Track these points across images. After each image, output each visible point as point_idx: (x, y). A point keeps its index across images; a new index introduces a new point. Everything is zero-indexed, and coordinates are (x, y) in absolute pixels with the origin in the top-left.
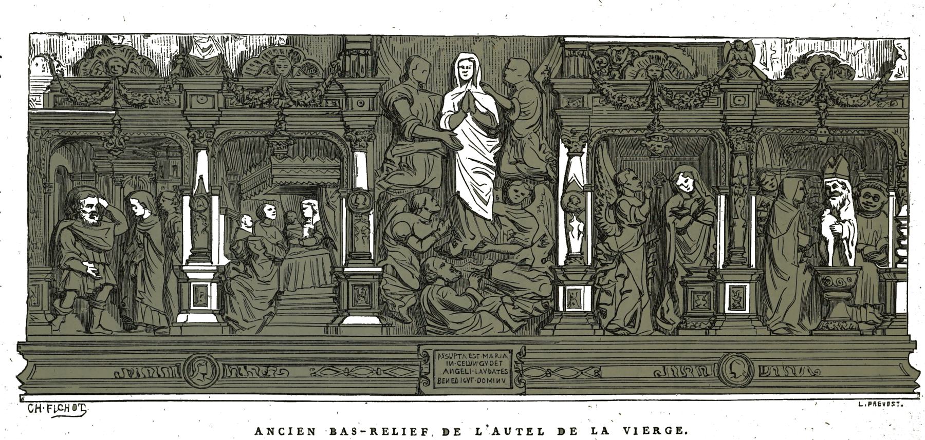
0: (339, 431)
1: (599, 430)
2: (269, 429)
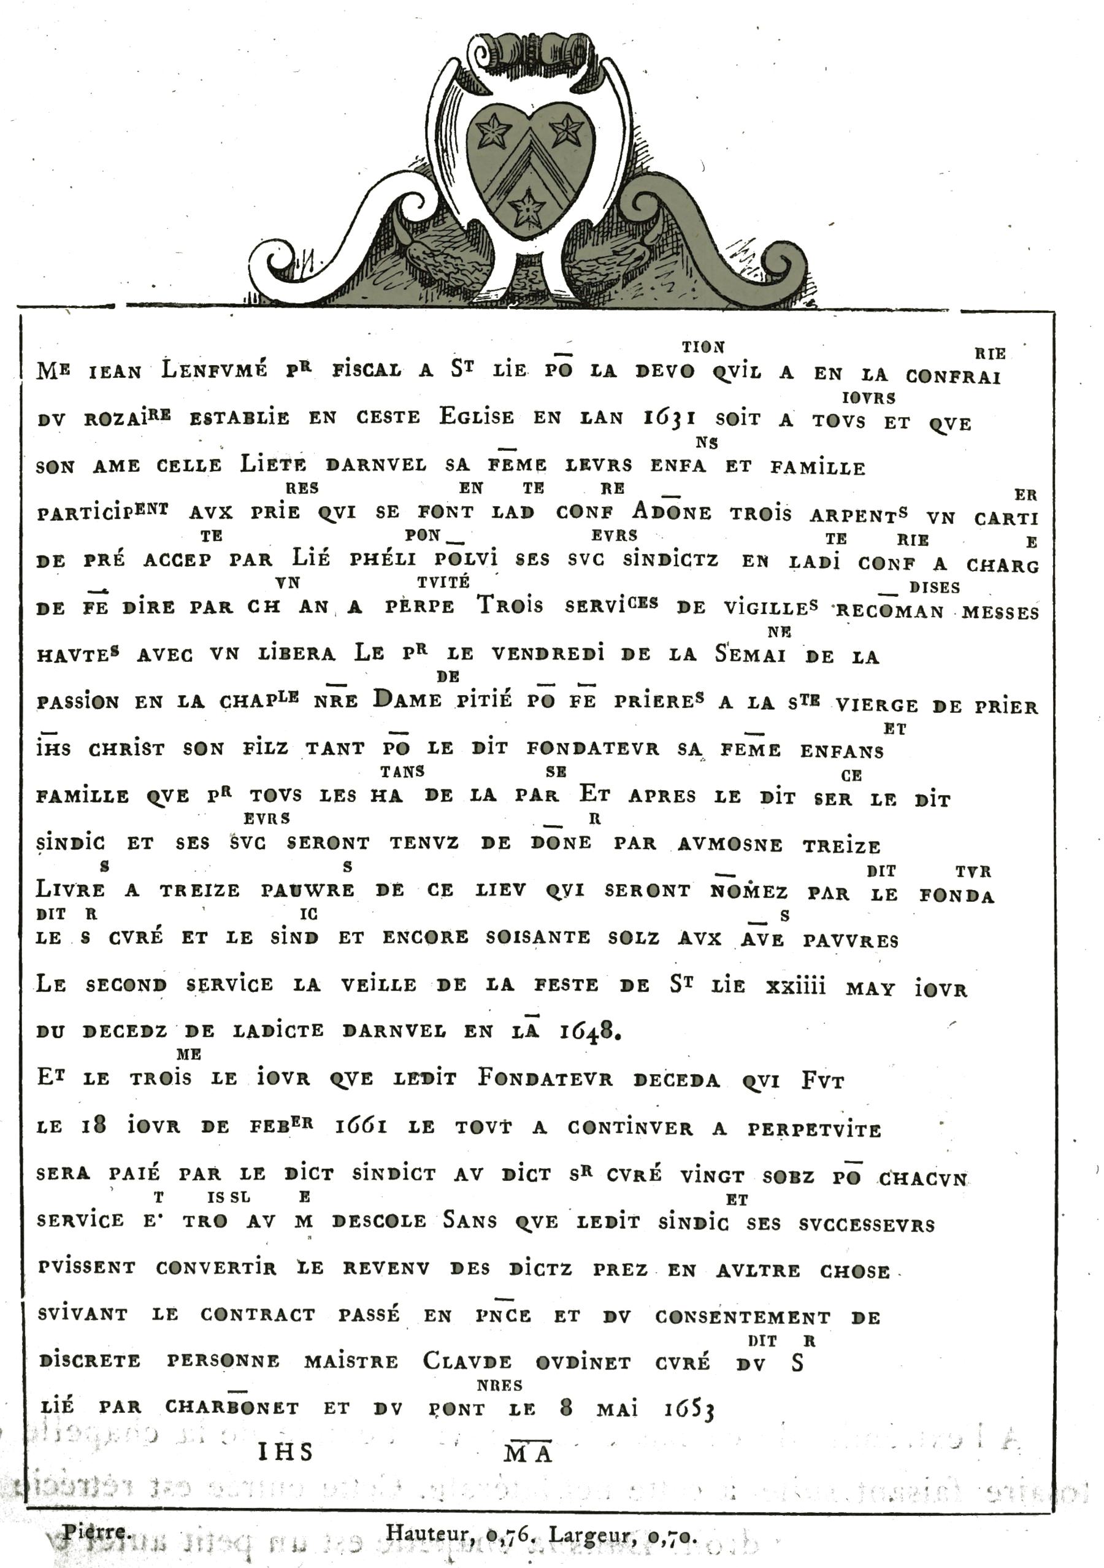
0: (274, 1314)
1: (499, 982)
2: (318, 698)
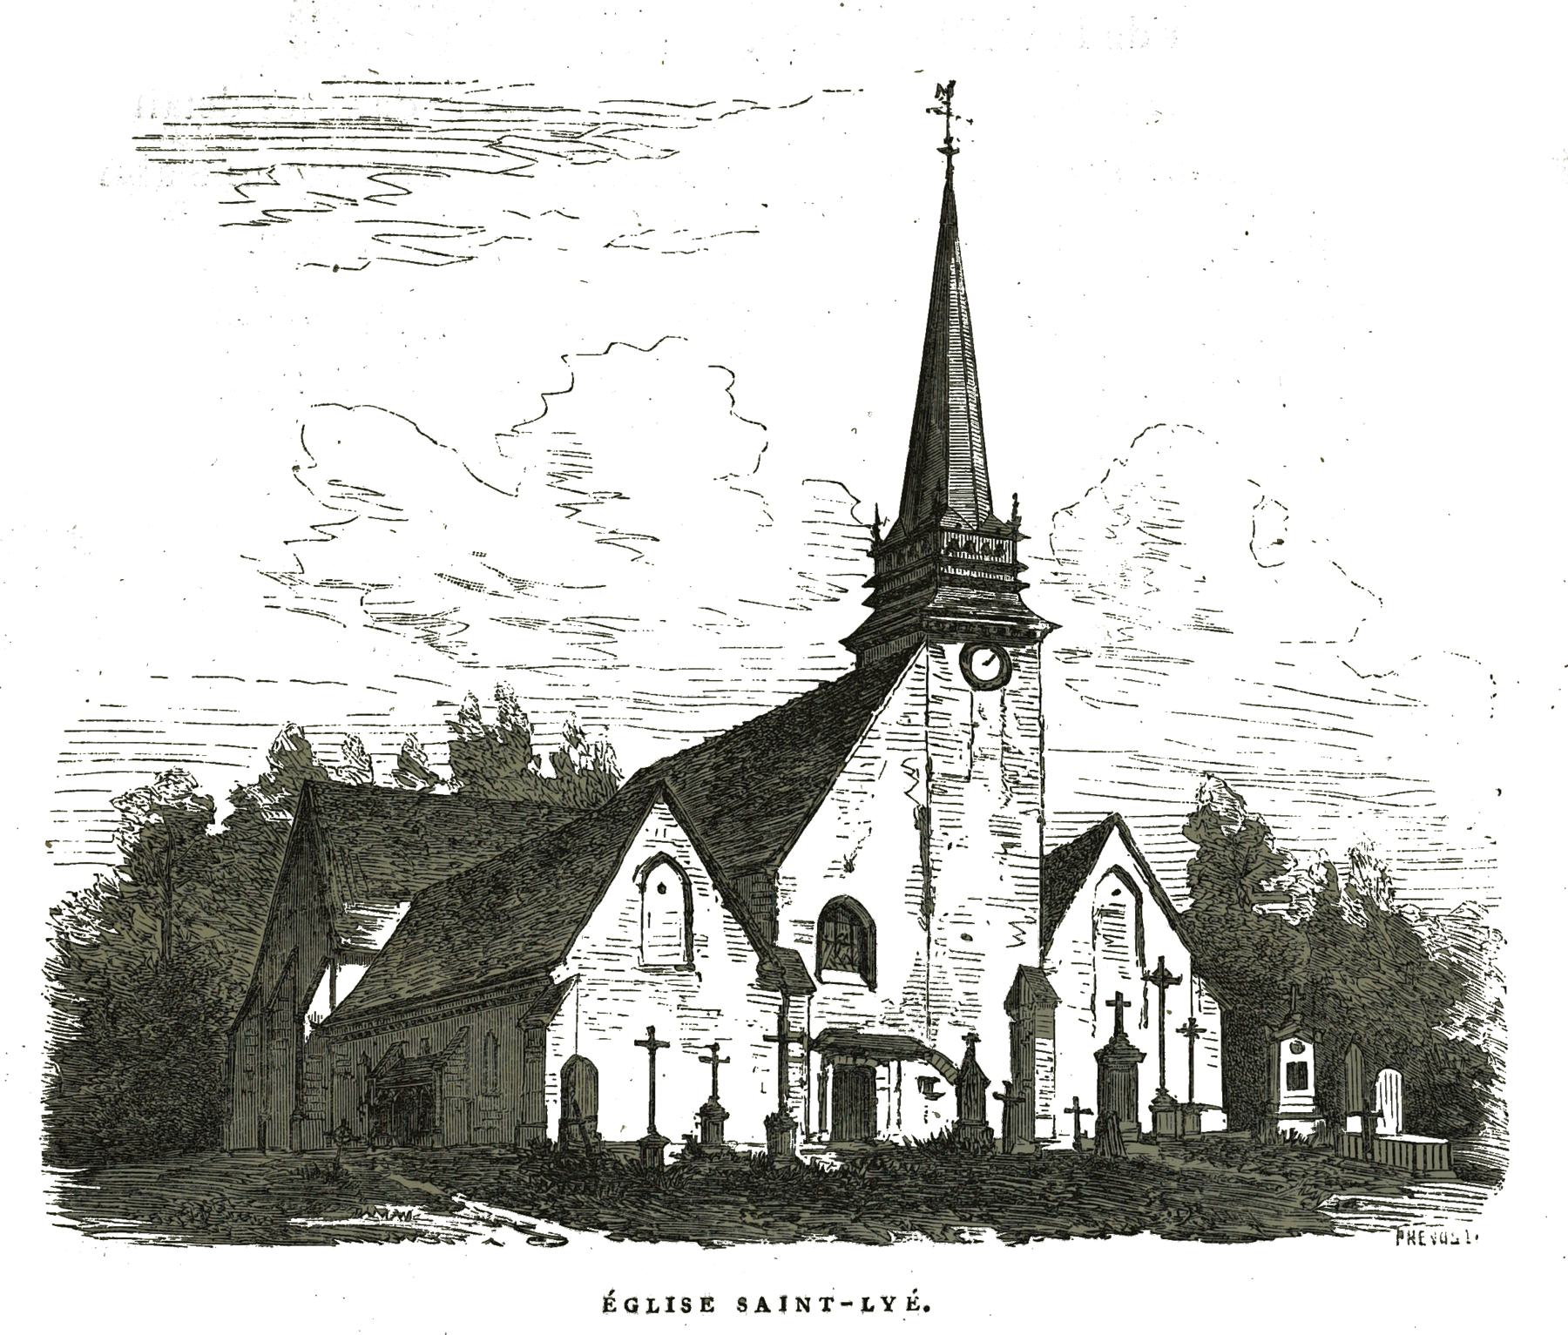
0: (753, 1304)
